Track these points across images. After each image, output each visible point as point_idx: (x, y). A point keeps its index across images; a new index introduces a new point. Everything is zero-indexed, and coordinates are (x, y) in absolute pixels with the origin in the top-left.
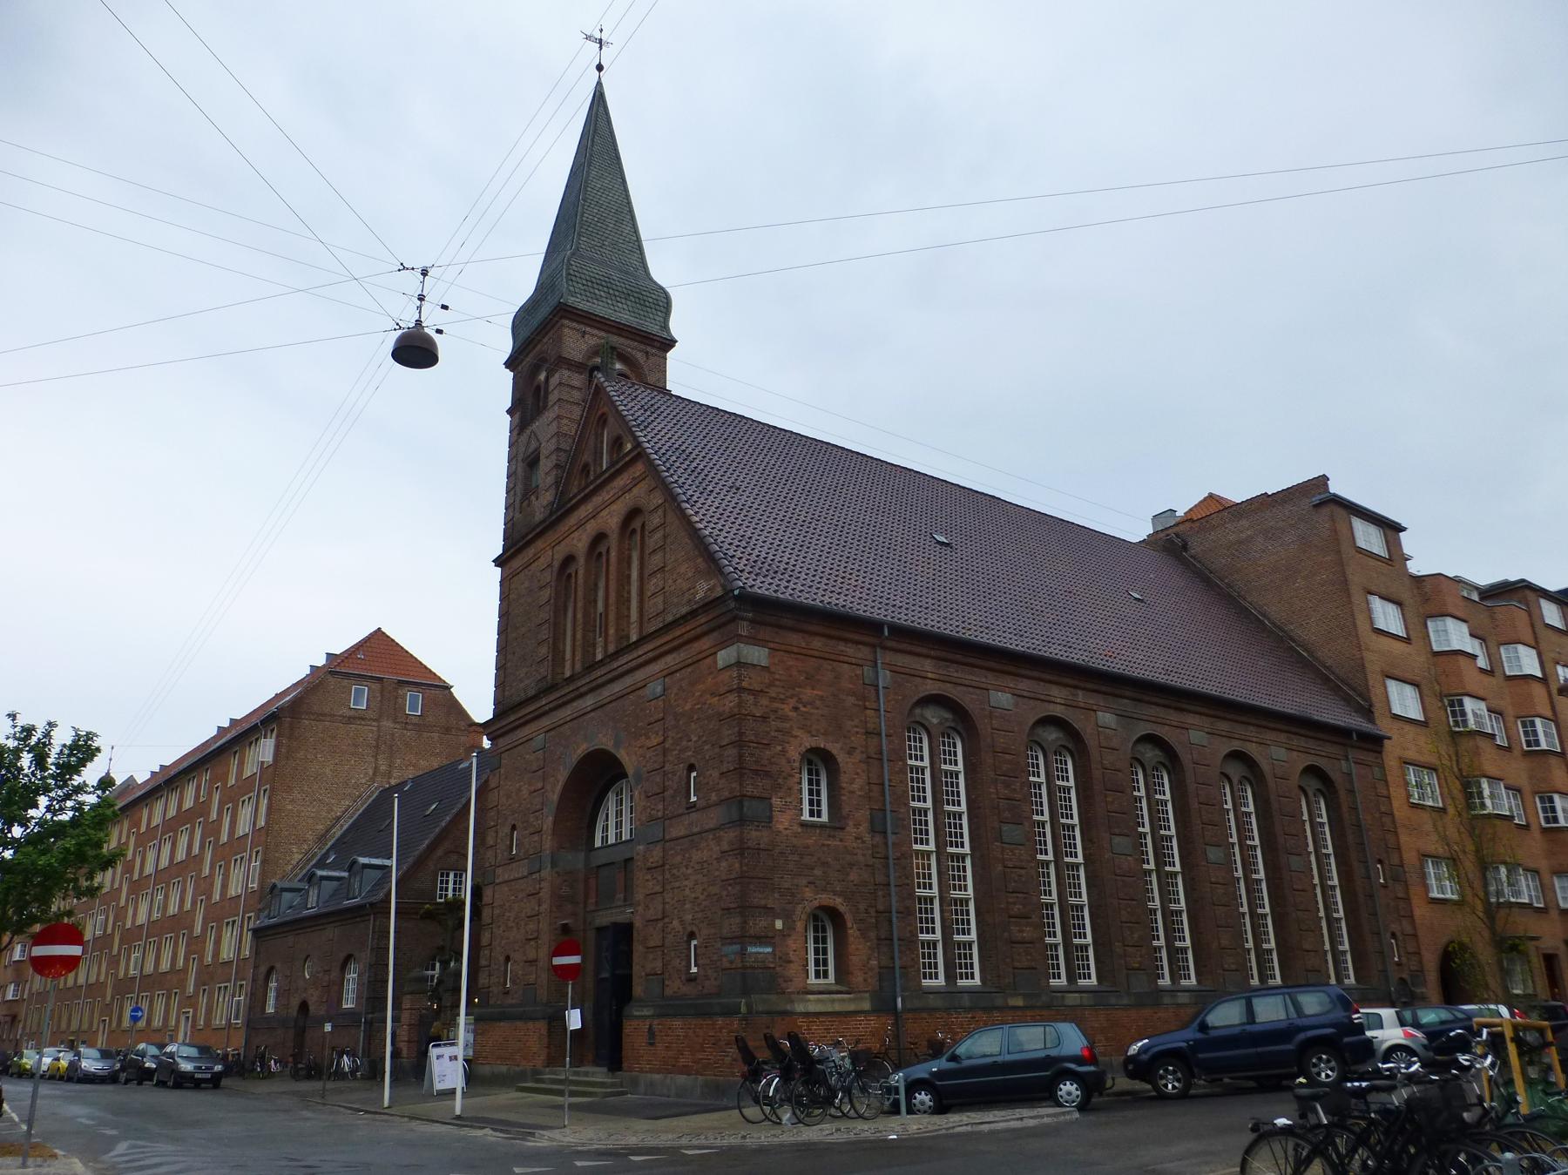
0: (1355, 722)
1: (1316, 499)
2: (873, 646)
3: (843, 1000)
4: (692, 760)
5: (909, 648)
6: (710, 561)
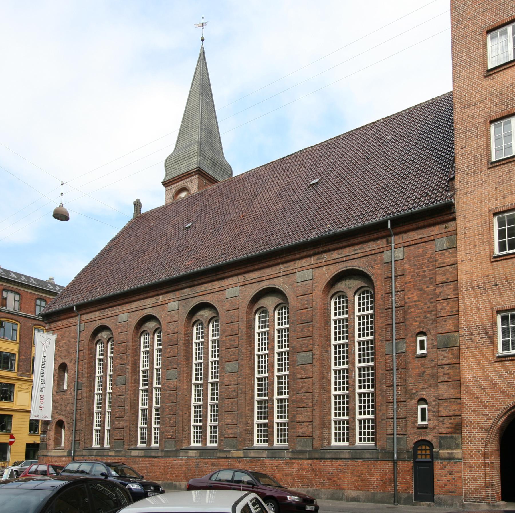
5: (265, 265)
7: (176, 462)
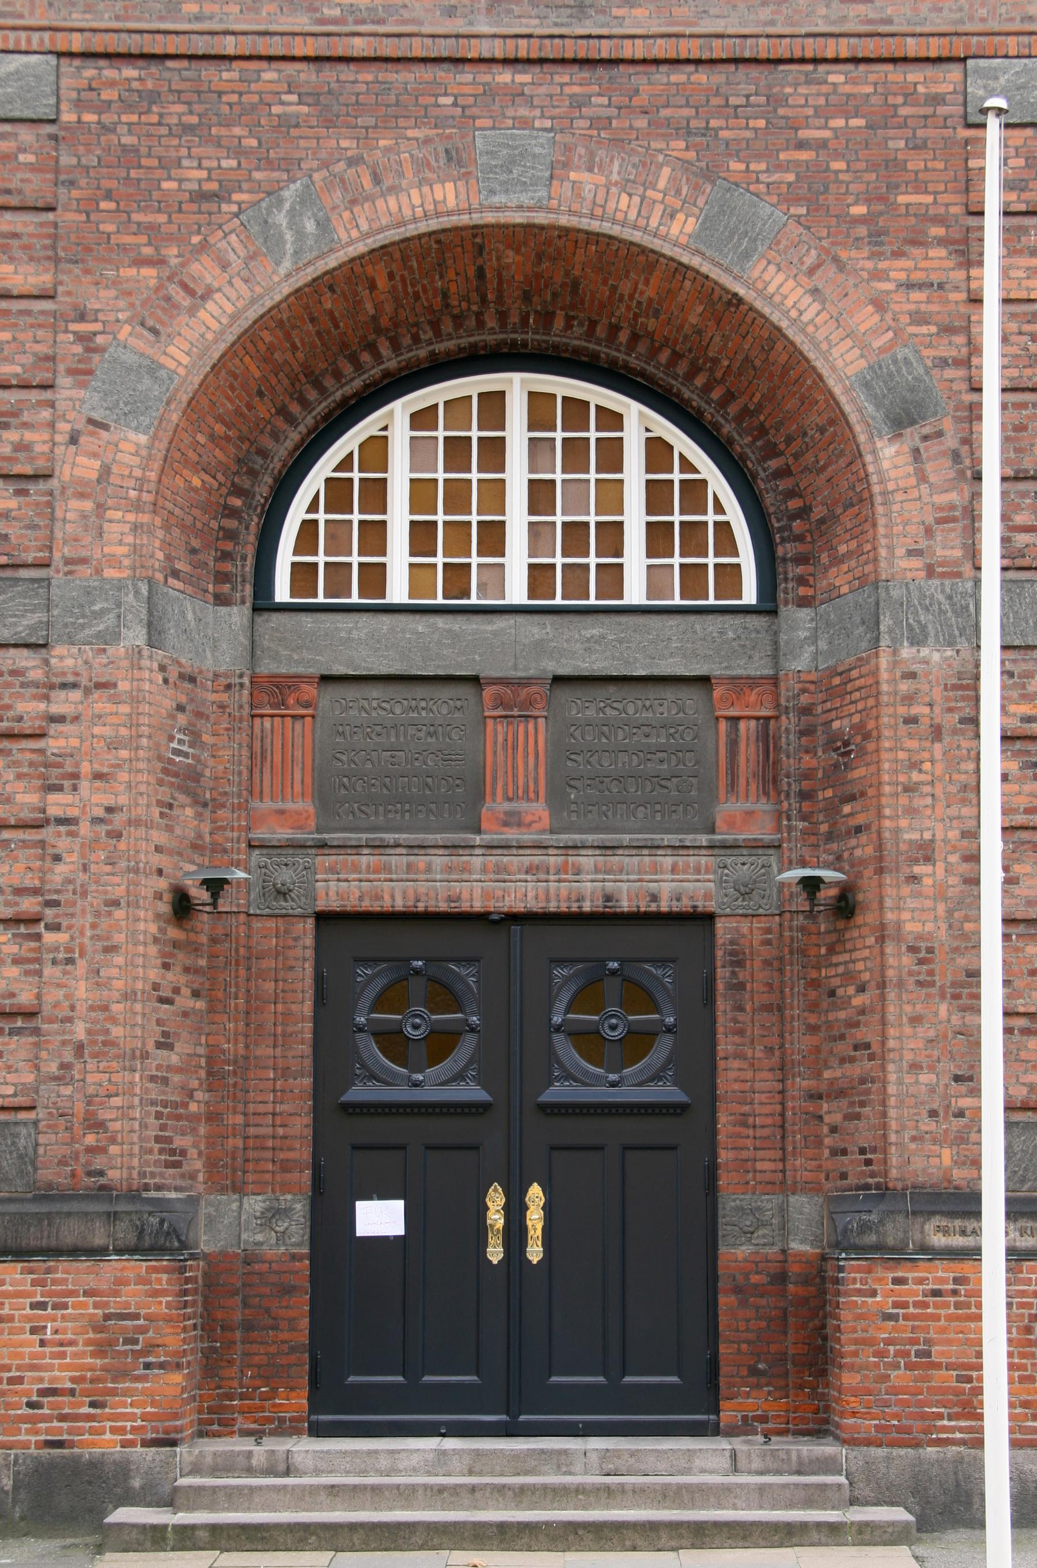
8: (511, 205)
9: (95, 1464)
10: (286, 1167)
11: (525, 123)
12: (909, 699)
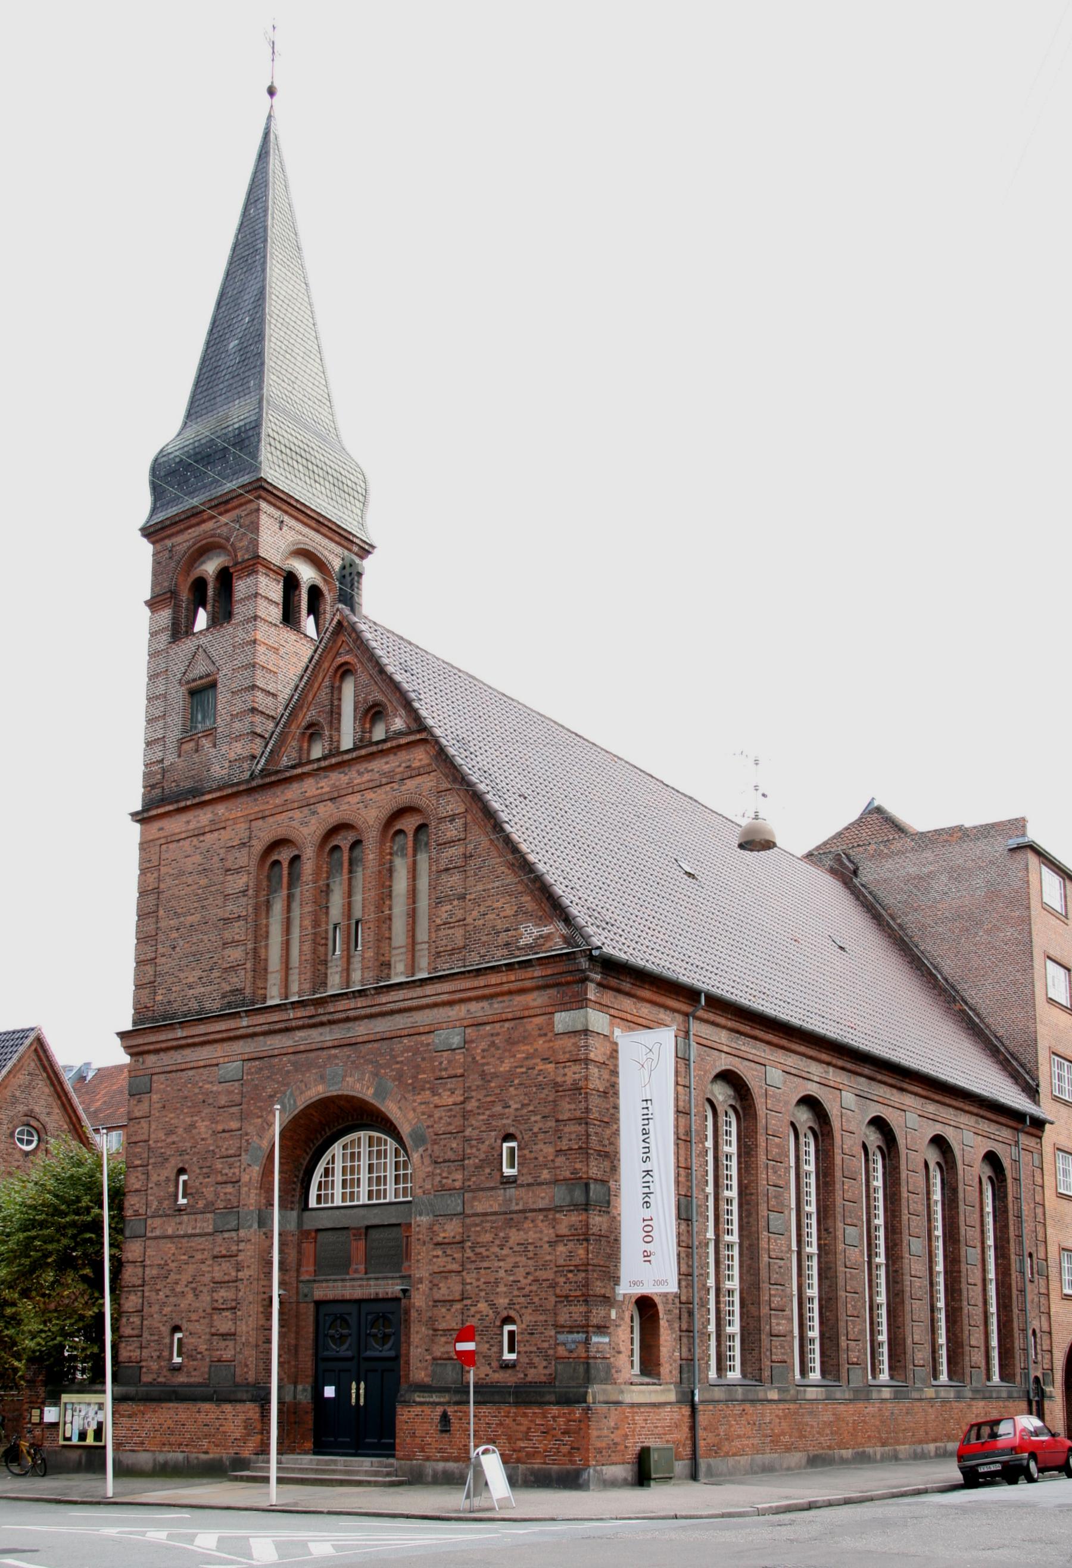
0: (1013, 1097)
1: (1013, 842)
2: (686, 1015)
3: (656, 1391)
4: (512, 1130)
6: (552, 906)
7: (867, 1410)
8: (334, 1091)
9: (244, 1459)
10: (307, 1376)
11: (337, 1065)
12: (418, 1233)
